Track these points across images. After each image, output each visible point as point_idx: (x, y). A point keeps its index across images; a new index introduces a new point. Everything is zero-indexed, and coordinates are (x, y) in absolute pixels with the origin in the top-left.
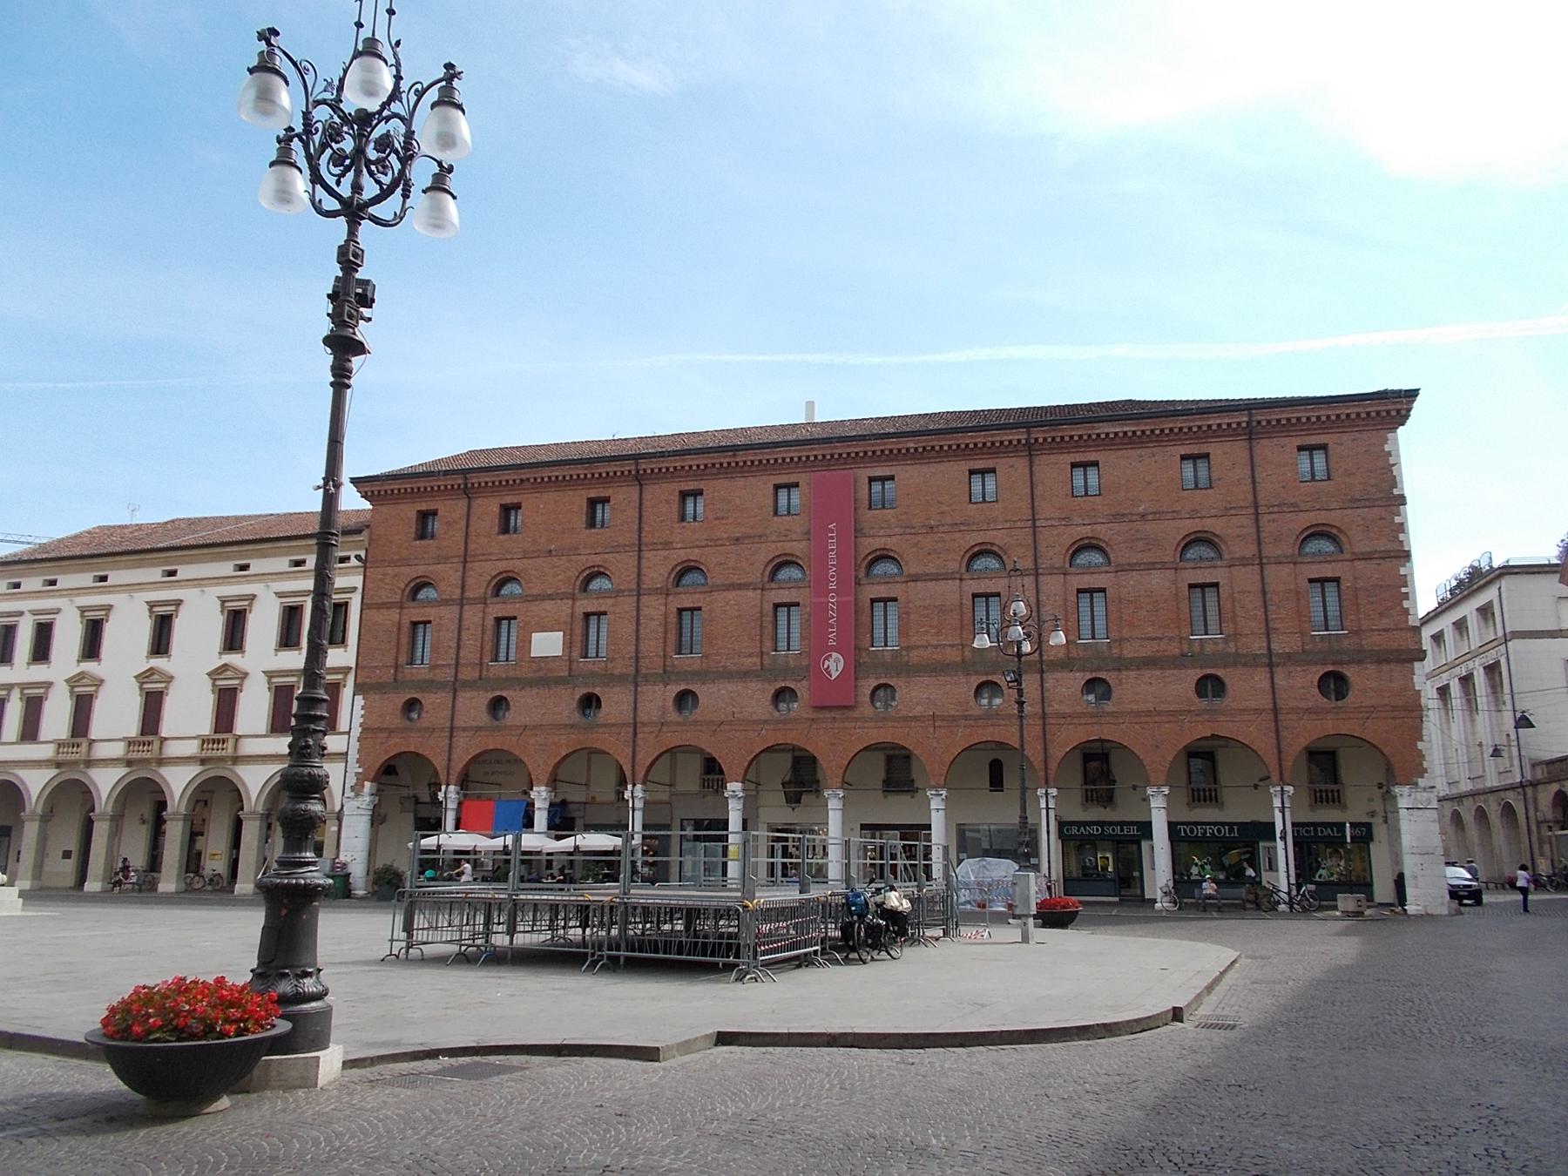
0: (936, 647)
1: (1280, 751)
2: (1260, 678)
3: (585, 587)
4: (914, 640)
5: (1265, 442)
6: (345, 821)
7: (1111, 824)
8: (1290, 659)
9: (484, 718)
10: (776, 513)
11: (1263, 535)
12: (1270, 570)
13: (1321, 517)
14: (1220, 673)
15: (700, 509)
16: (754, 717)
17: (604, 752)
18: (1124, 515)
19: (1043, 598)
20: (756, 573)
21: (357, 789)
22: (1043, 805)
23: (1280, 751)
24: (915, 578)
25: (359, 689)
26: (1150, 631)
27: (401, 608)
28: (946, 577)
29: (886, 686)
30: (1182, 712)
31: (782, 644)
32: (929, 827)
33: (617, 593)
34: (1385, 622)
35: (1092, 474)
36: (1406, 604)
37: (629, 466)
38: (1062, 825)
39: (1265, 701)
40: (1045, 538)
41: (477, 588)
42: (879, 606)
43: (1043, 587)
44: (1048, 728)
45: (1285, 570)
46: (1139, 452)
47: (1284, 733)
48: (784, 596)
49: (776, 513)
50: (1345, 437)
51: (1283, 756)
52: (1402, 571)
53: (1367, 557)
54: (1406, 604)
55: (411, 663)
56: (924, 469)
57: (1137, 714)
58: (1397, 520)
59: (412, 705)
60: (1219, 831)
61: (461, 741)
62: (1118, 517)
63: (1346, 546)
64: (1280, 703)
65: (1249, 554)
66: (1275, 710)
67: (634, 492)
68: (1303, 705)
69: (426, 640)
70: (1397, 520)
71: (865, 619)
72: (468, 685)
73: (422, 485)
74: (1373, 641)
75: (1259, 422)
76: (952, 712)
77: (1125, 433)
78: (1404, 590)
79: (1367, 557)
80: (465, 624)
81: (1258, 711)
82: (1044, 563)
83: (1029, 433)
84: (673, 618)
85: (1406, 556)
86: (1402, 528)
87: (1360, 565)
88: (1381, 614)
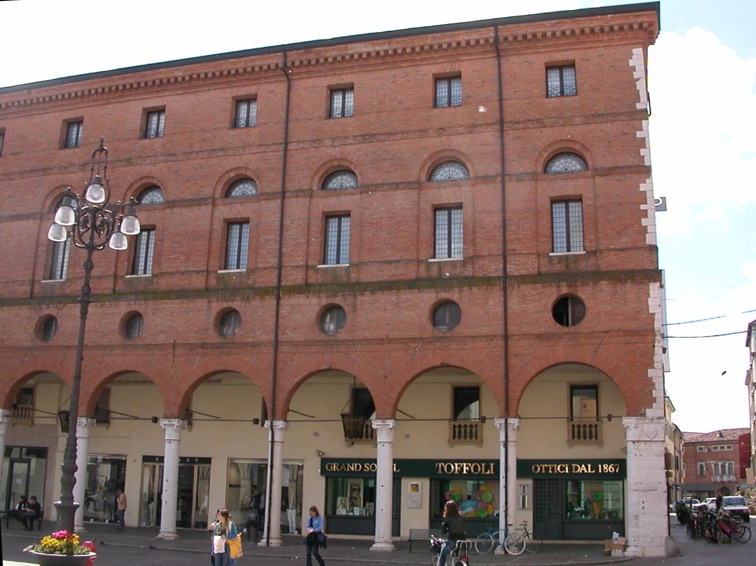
0: (183, 273)
1: (507, 381)
2: (493, 301)
3: (227, 193)
4: (165, 268)
5: (514, 59)
7: (352, 461)
8: (523, 279)
9: (548, 322)
10: (435, 105)
11: (506, 152)
12: (511, 186)
13: (566, 133)
14: (455, 297)
15: (253, 114)
16: (20, 344)
17: (240, 373)
18: (373, 135)
19: (287, 222)
20: (416, 172)
22: (502, 438)
23: (507, 381)
24: (376, 187)
26: (389, 255)
27: (311, 196)
28: (198, 202)
29: (337, 308)
30: (413, 340)
31: (233, 259)
32: (161, 459)
33: (261, 197)
34: (624, 241)
35: (568, 75)
36: (644, 222)
37: (278, 59)
38: (325, 462)
39: (497, 328)
40: (297, 158)
41: (301, 179)
42: (442, 216)
43: (288, 211)
44: (280, 356)
45: (304, 201)
46: (393, 72)
47: (513, 361)
48: (446, 196)
49: (435, 105)
50: (591, 53)
51: (511, 386)
52: (642, 188)
53: (609, 172)
54: (644, 222)
55: (134, 271)
56: (388, 74)
57: (368, 341)
58: (639, 134)
59: (225, 317)
60: (476, 468)
62: (367, 137)
63: (590, 163)
64: (512, 329)
65: (492, 172)
66: (506, 337)
67: (488, 64)
68: (534, 330)
69: (241, 242)
70: (639, 134)
71: (426, 228)
72: (101, 298)
73: (117, 83)
74: (610, 262)
75: (506, 39)
76: (191, 341)
77: (378, 53)
78: (643, 207)
79: (609, 172)
81: (490, 338)
82: (292, 186)
83: (286, 57)
84: (317, 223)
85: (647, 171)
86: (643, 143)
87: (599, 180)
88: (619, 233)
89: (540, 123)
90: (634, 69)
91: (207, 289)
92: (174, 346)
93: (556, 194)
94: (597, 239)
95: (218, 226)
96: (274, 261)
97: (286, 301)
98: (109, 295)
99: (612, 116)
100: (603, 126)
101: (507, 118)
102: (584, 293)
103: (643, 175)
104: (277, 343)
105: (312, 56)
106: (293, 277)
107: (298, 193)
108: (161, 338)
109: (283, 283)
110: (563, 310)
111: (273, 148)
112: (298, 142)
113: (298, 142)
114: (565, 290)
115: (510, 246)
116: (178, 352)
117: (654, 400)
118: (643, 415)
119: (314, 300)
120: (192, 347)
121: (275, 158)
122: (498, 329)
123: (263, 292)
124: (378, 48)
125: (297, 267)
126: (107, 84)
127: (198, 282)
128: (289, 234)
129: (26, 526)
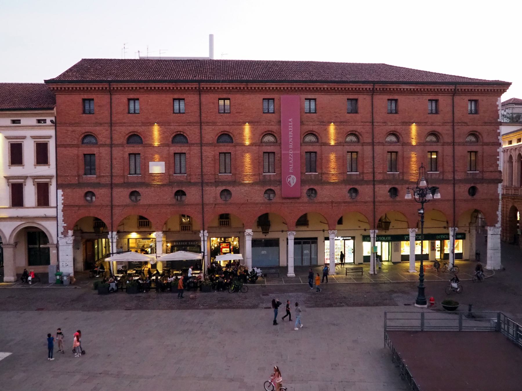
6: (60, 248)
8: (460, 181)
9: (466, 196)
16: (257, 202)
19: (375, 155)
21: (65, 234)
25: (58, 187)
34: (491, 169)
40: (377, 130)
42: (177, 157)
53: (487, 144)
58: (498, 131)
61: (116, 211)
70: (498, 131)
71: (127, 161)
76: (339, 200)
78: (498, 157)
80: (114, 156)
82: (376, 141)
83: (199, 85)
89: (466, 124)
90: (498, 106)
91: (79, 183)
92: (332, 202)
93: (265, 151)
94: (483, 167)
95: (126, 156)
96: (371, 170)
97: (377, 187)
98: (76, 184)
99: (490, 123)
100: (487, 127)
101: (455, 121)
102: (478, 186)
103: (496, 146)
104: (374, 202)
105: (186, 86)
106: (379, 177)
107: (118, 145)
108: (326, 199)
109: (375, 179)
110: (473, 191)
111: (367, 124)
112: (378, 122)
113: (378, 122)
114: (472, 185)
115: (456, 169)
116: (333, 205)
117: (498, 221)
118: (495, 226)
119: (387, 186)
120: (339, 203)
121: (368, 128)
122: (452, 198)
123: (367, 182)
124: (411, 87)
125: (380, 173)
126: (289, 86)
127: (75, 181)
128: (376, 160)
129: (23, 281)
